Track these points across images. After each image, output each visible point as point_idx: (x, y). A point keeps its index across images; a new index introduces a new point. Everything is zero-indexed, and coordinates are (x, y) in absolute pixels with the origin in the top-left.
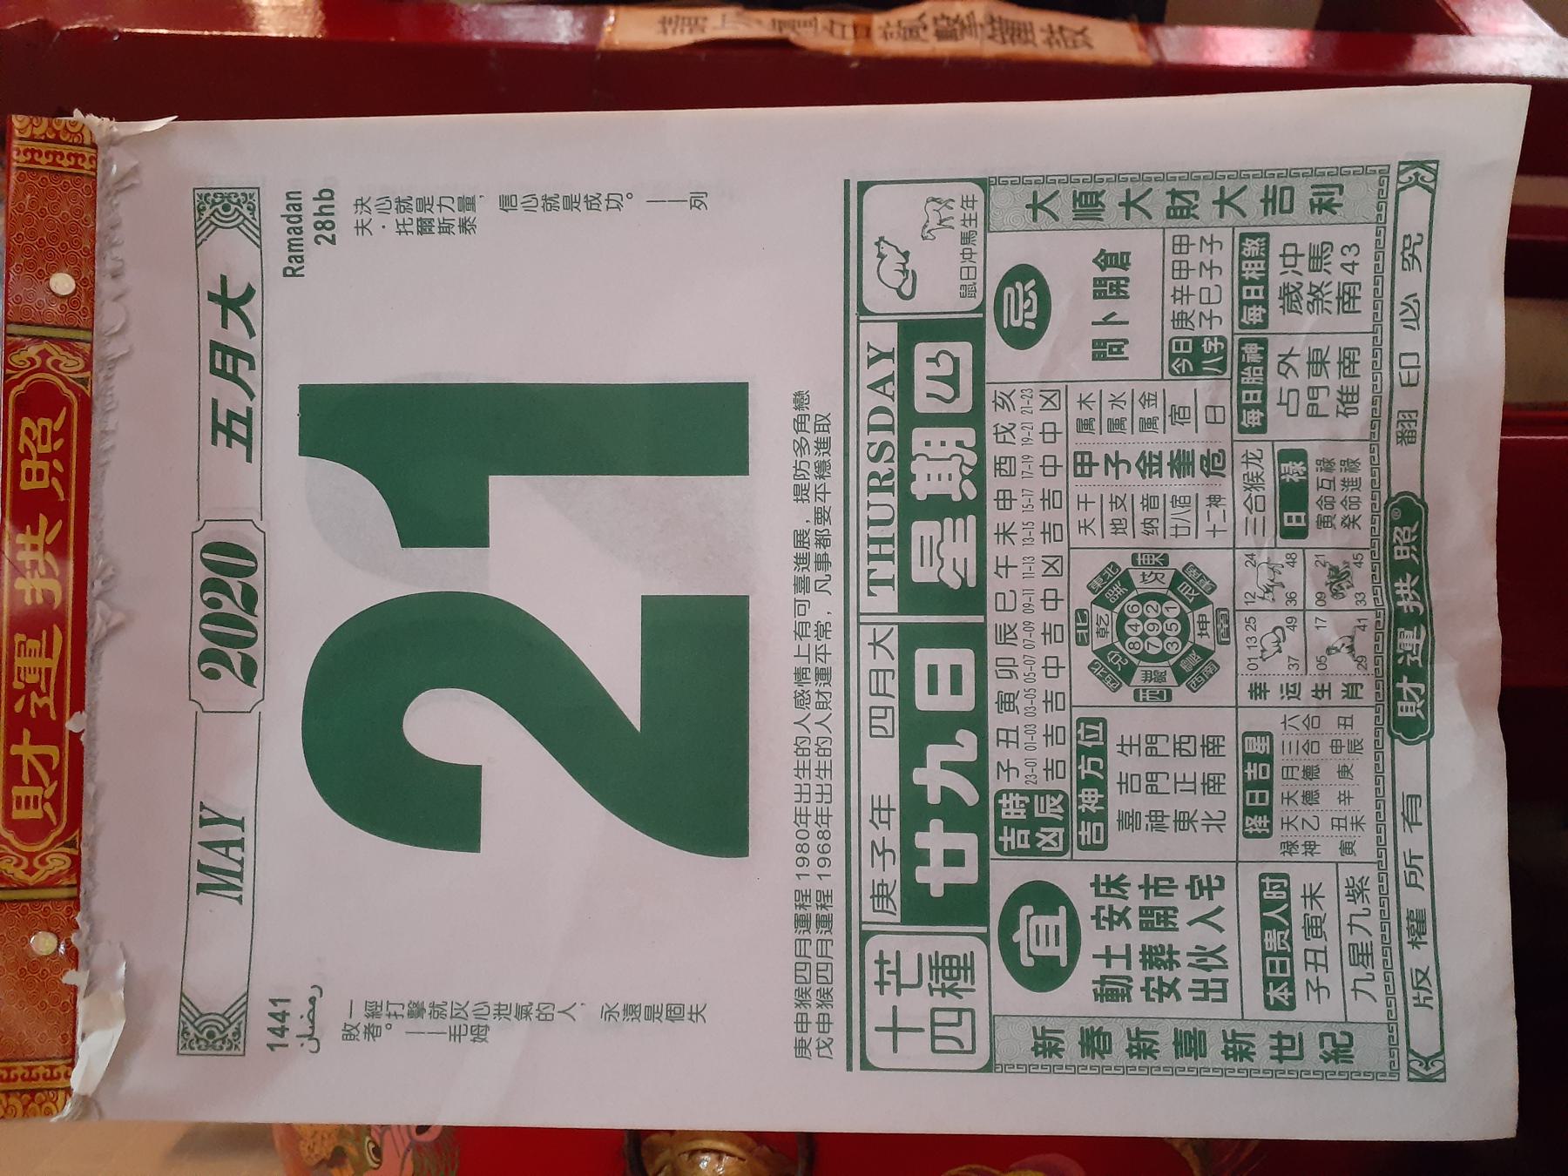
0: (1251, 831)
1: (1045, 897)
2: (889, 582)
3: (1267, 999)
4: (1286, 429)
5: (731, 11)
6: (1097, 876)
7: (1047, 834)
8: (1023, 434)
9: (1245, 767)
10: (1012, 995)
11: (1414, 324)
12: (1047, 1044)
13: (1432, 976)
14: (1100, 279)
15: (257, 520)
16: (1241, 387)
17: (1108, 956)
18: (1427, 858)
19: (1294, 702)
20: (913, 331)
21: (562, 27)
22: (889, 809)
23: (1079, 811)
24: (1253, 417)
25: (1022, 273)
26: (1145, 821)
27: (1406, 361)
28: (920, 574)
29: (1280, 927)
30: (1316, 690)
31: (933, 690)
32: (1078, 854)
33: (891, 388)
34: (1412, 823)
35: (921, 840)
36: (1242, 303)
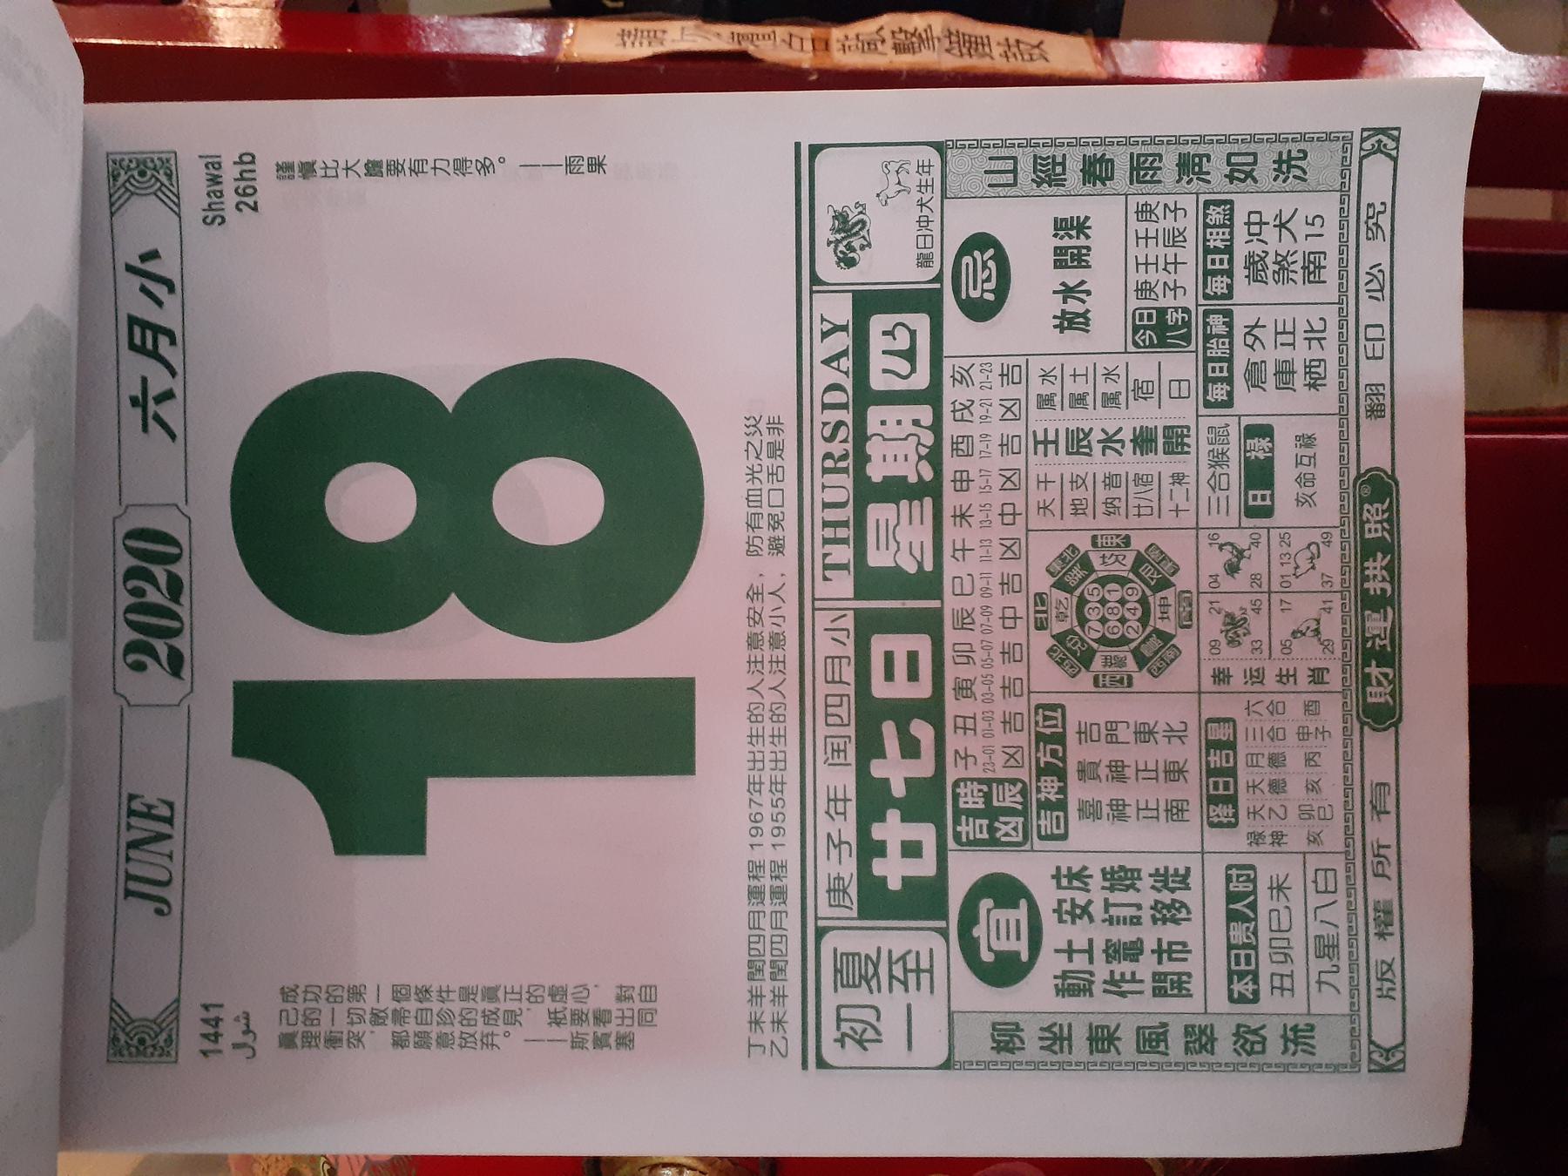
0: (1216, 820)
1: (1005, 891)
2: (844, 567)
3: (1230, 991)
4: (1251, 404)
5: (690, 24)
6: (1058, 868)
7: (1006, 824)
8: (982, 418)
9: (1208, 754)
10: (973, 994)
11: (1379, 295)
12: (1006, 1038)
13: (1397, 967)
14: (1061, 248)
15: (181, 505)
16: (1207, 360)
17: (1070, 951)
18: (1394, 848)
19: (1257, 687)
20: (868, 303)
21: (526, 40)
22: (845, 800)
23: (1038, 800)
24: (1219, 392)
25: (980, 242)
26: (1106, 810)
27: (1372, 333)
28: (877, 558)
29: (1247, 919)
30: (1281, 676)
31: (889, 676)
32: (1037, 844)
33: (846, 363)
34: (1380, 812)
35: (877, 832)
36: (1207, 273)
